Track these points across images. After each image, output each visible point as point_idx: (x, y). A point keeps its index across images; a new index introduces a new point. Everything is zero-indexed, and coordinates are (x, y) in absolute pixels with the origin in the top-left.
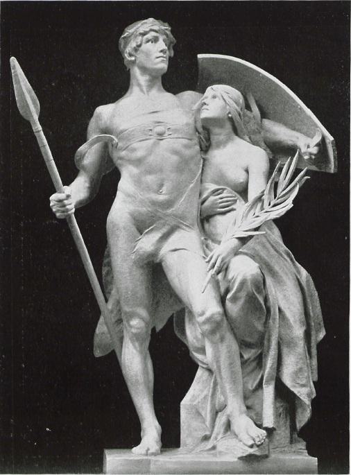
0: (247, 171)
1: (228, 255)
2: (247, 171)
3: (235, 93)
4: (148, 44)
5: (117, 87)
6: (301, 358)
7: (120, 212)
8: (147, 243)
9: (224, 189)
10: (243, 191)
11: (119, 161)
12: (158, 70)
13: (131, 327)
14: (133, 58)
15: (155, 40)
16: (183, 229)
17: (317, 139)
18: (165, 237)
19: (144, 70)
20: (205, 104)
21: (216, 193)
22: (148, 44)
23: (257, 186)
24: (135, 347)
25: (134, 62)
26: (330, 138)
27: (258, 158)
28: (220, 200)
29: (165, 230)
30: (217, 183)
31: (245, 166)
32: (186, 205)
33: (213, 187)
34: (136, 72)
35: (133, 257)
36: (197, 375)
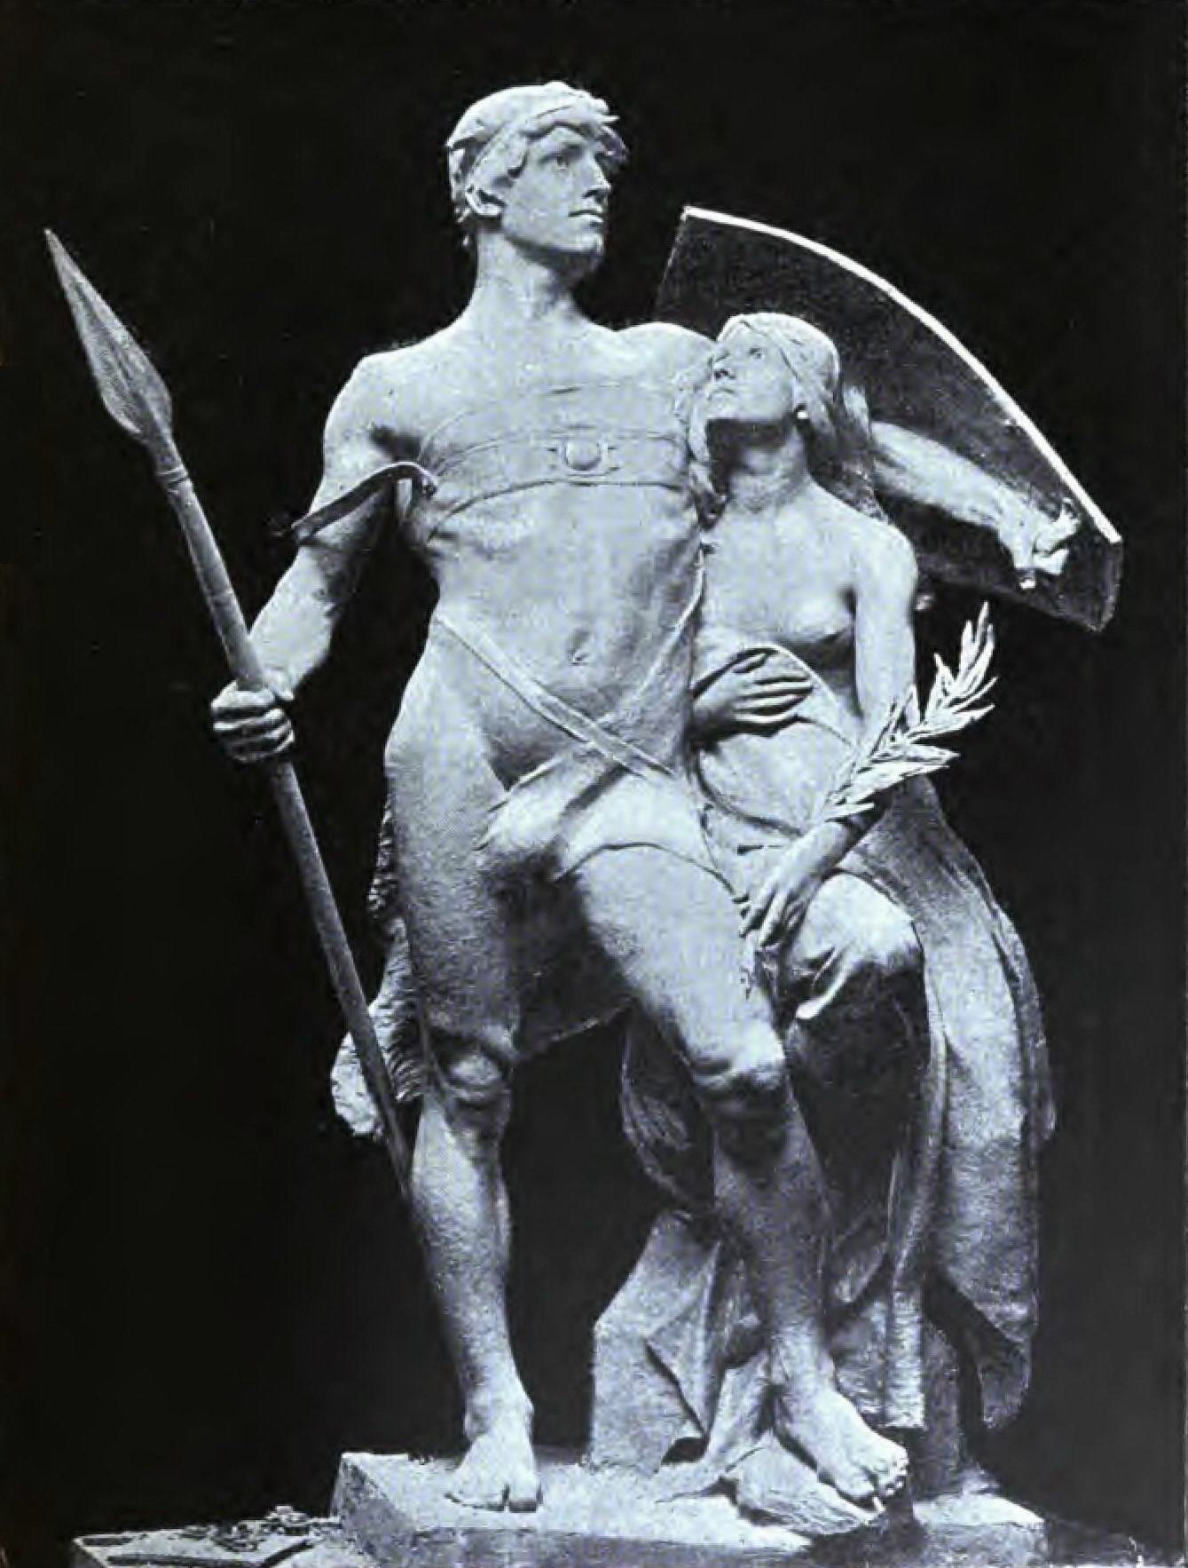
0: (850, 599)
1: (803, 885)
2: (850, 599)
3: (819, 344)
4: (534, 149)
5: (424, 283)
6: (1010, 1211)
7: (435, 719)
8: (525, 818)
9: (770, 652)
10: (834, 657)
11: (436, 544)
12: (575, 257)
13: (457, 1082)
14: (493, 210)
15: (568, 155)
16: (809, 901)
17: (1066, 525)
18: (589, 796)
19: (533, 251)
20: (726, 373)
21: (743, 665)
22: (534, 149)
23: (886, 648)
24: (462, 1146)
25: (494, 224)
26: (1053, 613)
27: (889, 563)
28: (759, 689)
29: (584, 777)
30: (745, 627)
31: (843, 580)
32: (652, 688)
33: (737, 643)
34: (495, 253)
35: (480, 862)
36: (518, 1384)
